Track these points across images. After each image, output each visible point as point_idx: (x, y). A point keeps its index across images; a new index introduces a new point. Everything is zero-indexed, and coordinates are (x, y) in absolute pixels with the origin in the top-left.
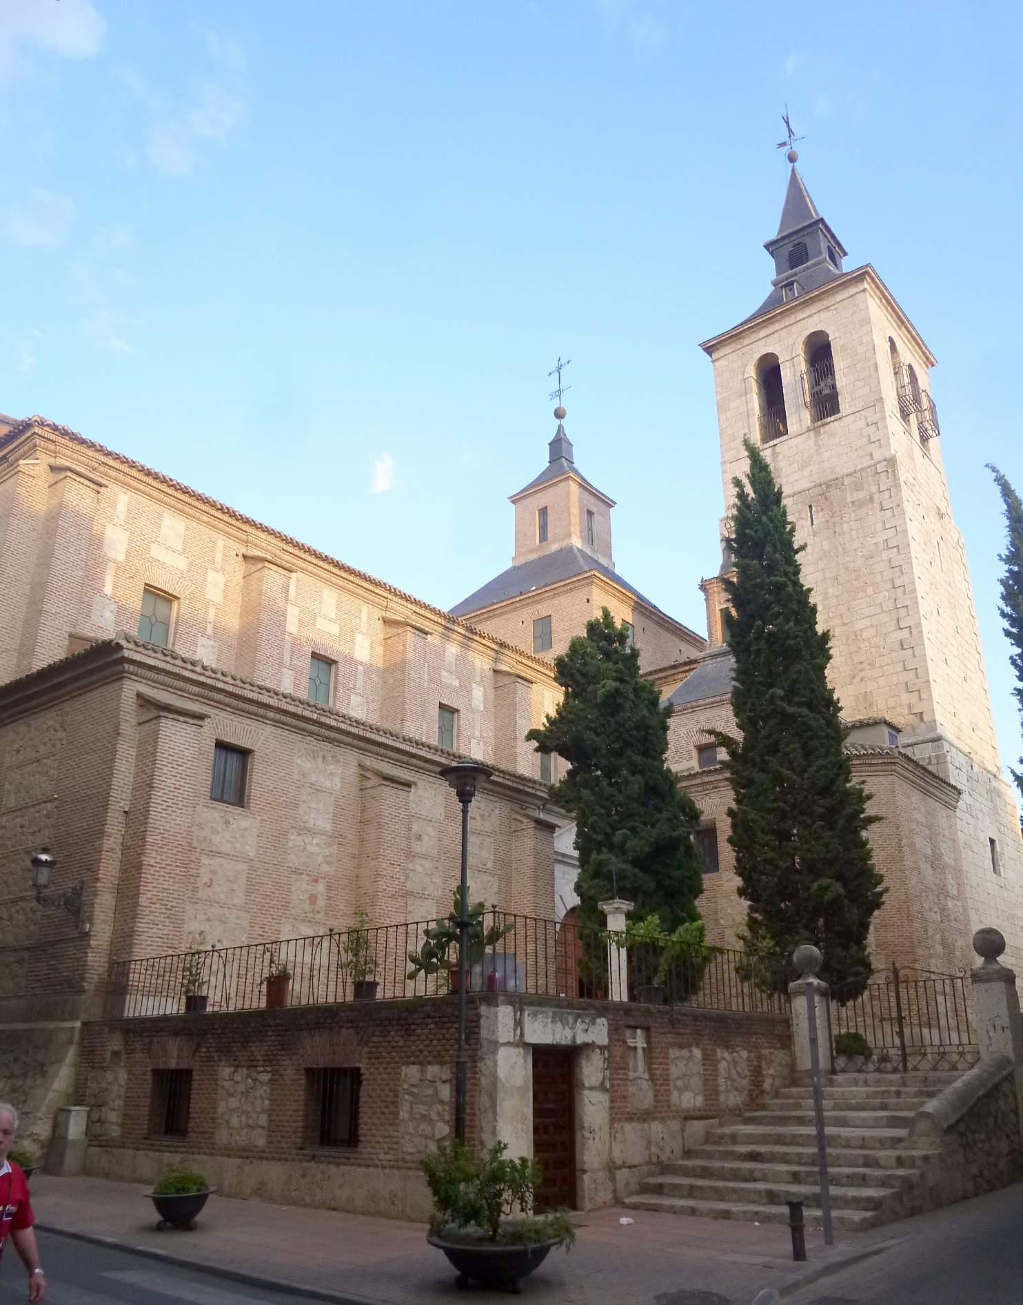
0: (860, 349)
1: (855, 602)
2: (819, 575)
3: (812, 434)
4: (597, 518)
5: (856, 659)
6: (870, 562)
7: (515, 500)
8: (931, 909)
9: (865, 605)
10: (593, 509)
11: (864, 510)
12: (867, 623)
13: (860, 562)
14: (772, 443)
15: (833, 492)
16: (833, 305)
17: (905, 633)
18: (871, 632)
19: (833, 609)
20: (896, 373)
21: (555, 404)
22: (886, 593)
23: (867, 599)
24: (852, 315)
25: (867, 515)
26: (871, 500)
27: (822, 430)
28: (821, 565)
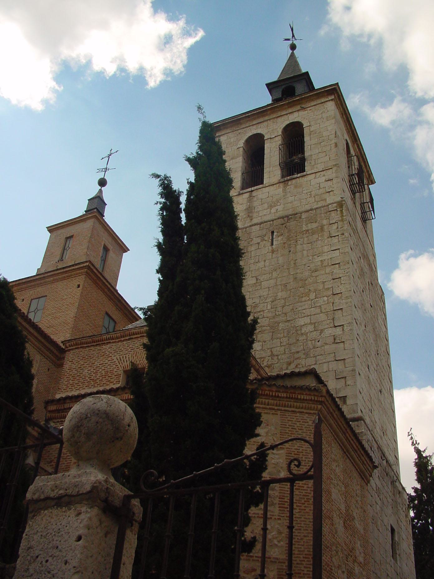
0: (325, 134)
1: (300, 304)
2: (272, 282)
3: (281, 185)
4: (111, 254)
5: (294, 349)
6: (317, 274)
7: (51, 229)
8: (339, 567)
9: (306, 307)
10: (110, 246)
11: (316, 236)
12: (307, 320)
13: (307, 274)
14: (250, 189)
15: (292, 224)
16: (309, 107)
17: (338, 331)
18: (311, 328)
19: (279, 309)
20: (349, 167)
21: (101, 175)
22: (325, 298)
23: (309, 302)
24: (322, 113)
25: (317, 240)
26: (322, 229)
27: (290, 183)
28: (275, 274)
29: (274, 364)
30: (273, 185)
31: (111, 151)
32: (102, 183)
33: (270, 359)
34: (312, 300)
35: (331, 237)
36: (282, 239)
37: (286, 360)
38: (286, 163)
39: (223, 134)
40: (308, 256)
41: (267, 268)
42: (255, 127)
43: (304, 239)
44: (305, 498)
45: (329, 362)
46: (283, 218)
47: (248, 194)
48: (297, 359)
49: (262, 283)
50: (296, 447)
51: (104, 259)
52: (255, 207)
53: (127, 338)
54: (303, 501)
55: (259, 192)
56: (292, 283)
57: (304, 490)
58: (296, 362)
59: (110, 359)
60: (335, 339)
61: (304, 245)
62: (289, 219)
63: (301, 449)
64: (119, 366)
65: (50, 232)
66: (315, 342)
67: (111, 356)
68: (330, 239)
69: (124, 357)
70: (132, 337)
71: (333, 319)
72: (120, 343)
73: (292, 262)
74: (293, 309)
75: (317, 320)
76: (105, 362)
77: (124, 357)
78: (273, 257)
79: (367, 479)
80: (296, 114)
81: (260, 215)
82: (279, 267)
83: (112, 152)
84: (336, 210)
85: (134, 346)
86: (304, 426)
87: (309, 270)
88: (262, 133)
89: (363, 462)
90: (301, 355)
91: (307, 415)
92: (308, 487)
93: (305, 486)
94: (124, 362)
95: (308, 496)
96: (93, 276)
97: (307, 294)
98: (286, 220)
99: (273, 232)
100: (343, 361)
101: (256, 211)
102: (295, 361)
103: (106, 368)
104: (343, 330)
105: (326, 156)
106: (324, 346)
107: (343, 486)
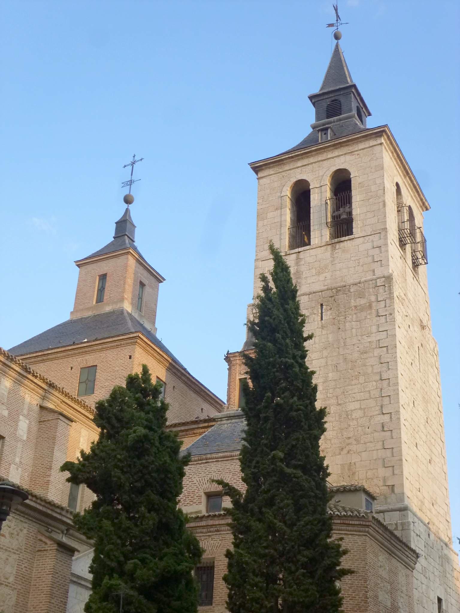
1: (349, 387)
3: (329, 247)
4: (147, 289)
5: (346, 434)
6: (365, 356)
9: (356, 391)
12: (357, 405)
13: (356, 355)
14: (297, 250)
15: (341, 297)
16: (357, 151)
21: (125, 191)
22: (374, 383)
23: (359, 386)
25: (366, 318)
26: (370, 307)
27: (338, 246)
29: (328, 448)
30: (321, 247)
31: (134, 157)
32: (128, 200)
33: (324, 443)
34: (361, 384)
35: (379, 316)
36: (331, 314)
37: (338, 445)
38: (335, 236)
39: (266, 176)
40: (357, 336)
41: (317, 346)
42: (299, 170)
43: (352, 316)
44: (358, 606)
45: (377, 450)
46: (332, 290)
47: (295, 255)
48: (349, 444)
49: (313, 361)
50: (349, 565)
51: (141, 297)
52: (302, 272)
53: (204, 461)
54: (356, 610)
55: (307, 253)
56: (342, 364)
57: (356, 600)
58: (348, 448)
59: (190, 480)
60: (383, 427)
61: (353, 322)
62: (338, 291)
63: (353, 566)
64: (199, 487)
65: (79, 267)
66: (365, 428)
67: (192, 478)
68: (378, 318)
69: (203, 480)
70: (208, 461)
71: (382, 407)
72: (198, 466)
73: (342, 342)
74: (344, 392)
75: (367, 406)
76: (186, 483)
77: (203, 480)
78: (323, 333)
79: (411, 567)
80: (342, 159)
81: (308, 282)
82: (329, 345)
83: (137, 158)
84: (384, 285)
85: (211, 470)
86: (355, 546)
87: (358, 351)
88: (307, 179)
89: (407, 556)
90: (352, 441)
91: (357, 537)
92: (359, 598)
93: (357, 597)
94: (203, 484)
95: (360, 604)
96: (143, 345)
97: (357, 378)
98: (335, 292)
99: (322, 305)
100: (391, 449)
101: (304, 277)
102: (347, 447)
103: (188, 489)
104: (391, 418)
105: (374, 216)
106: (373, 433)
107: (389, 585)
